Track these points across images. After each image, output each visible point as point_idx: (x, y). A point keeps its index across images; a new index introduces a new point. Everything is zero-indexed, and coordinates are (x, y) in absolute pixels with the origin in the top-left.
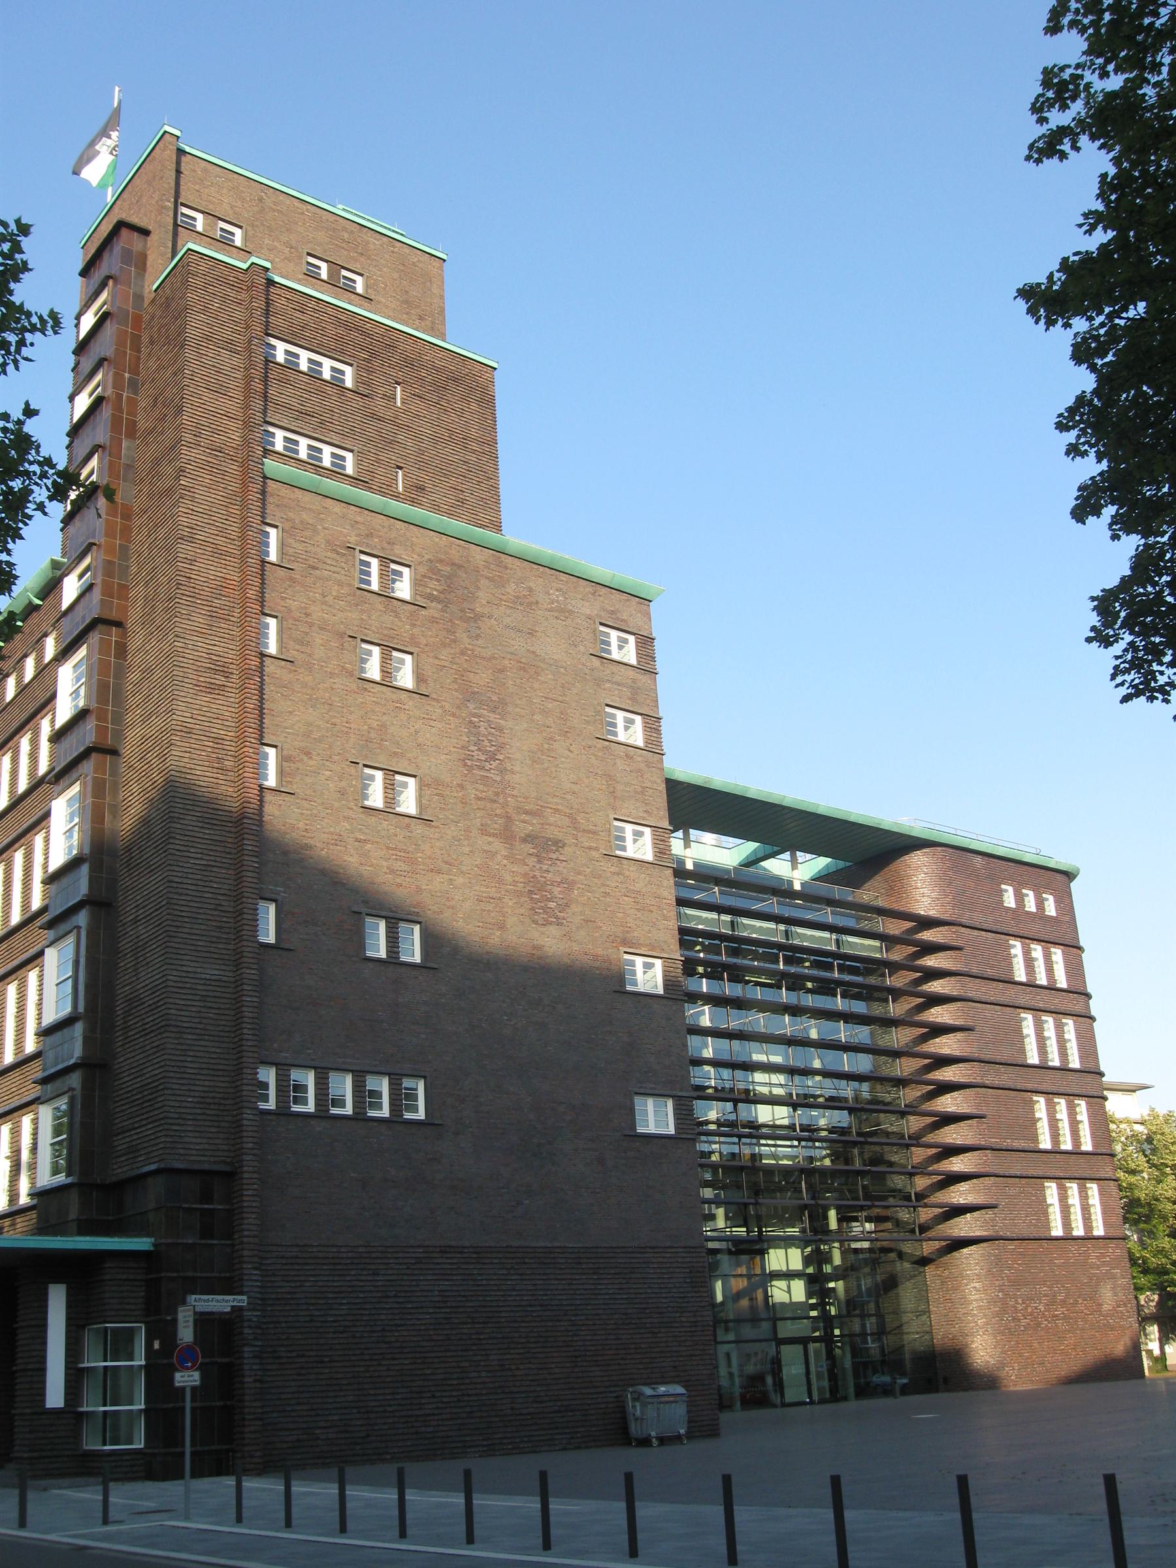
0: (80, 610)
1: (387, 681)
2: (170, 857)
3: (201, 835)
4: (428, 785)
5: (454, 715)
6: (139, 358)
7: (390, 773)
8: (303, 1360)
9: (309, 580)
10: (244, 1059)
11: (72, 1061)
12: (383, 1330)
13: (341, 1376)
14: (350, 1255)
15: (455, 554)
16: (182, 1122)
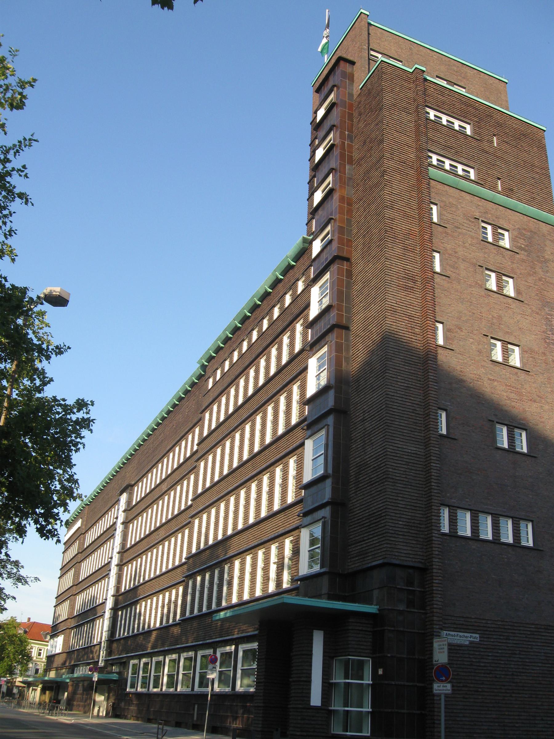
0: (324, 255)
1: (500, 291)
2: (387, 380)
3: (404, 369)
4: (526, 351)
5: (537, 313)
6: (352, 125)
7: (505, 343)
8: (466, 689)
9: (456, 234)
10: (433, 501)
11: (325, 501)
12: (513, 675)
13: (488, 701)
14: (493, 626)
15: (532, 224)
16: (396, 536)
